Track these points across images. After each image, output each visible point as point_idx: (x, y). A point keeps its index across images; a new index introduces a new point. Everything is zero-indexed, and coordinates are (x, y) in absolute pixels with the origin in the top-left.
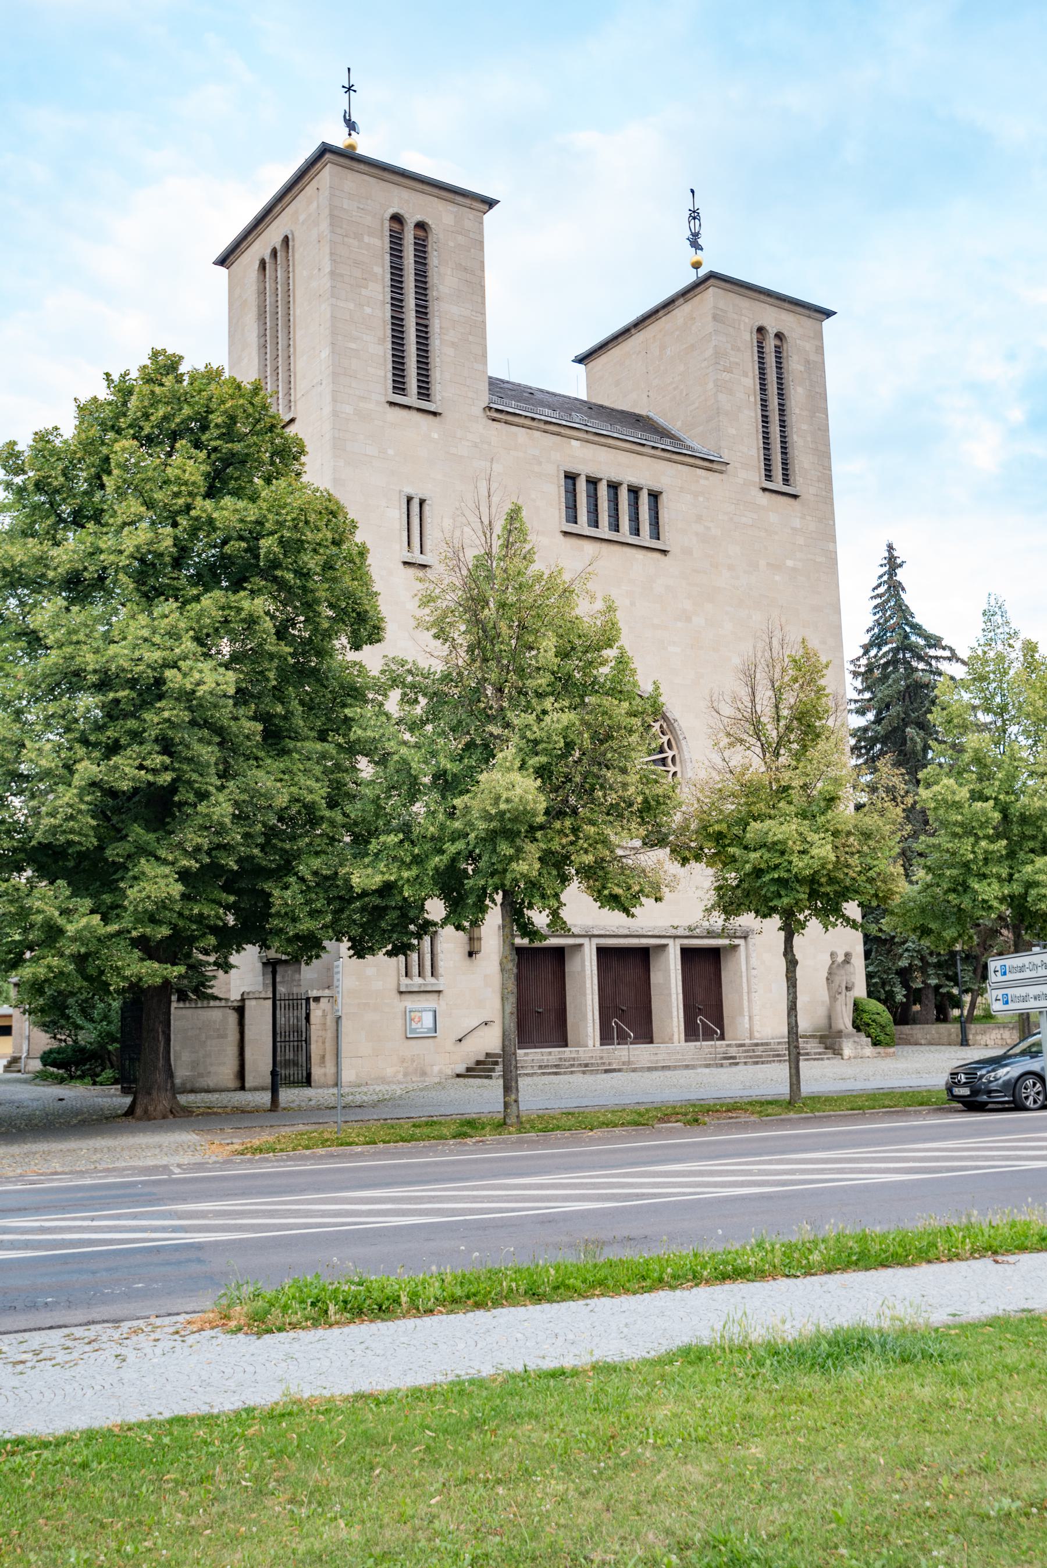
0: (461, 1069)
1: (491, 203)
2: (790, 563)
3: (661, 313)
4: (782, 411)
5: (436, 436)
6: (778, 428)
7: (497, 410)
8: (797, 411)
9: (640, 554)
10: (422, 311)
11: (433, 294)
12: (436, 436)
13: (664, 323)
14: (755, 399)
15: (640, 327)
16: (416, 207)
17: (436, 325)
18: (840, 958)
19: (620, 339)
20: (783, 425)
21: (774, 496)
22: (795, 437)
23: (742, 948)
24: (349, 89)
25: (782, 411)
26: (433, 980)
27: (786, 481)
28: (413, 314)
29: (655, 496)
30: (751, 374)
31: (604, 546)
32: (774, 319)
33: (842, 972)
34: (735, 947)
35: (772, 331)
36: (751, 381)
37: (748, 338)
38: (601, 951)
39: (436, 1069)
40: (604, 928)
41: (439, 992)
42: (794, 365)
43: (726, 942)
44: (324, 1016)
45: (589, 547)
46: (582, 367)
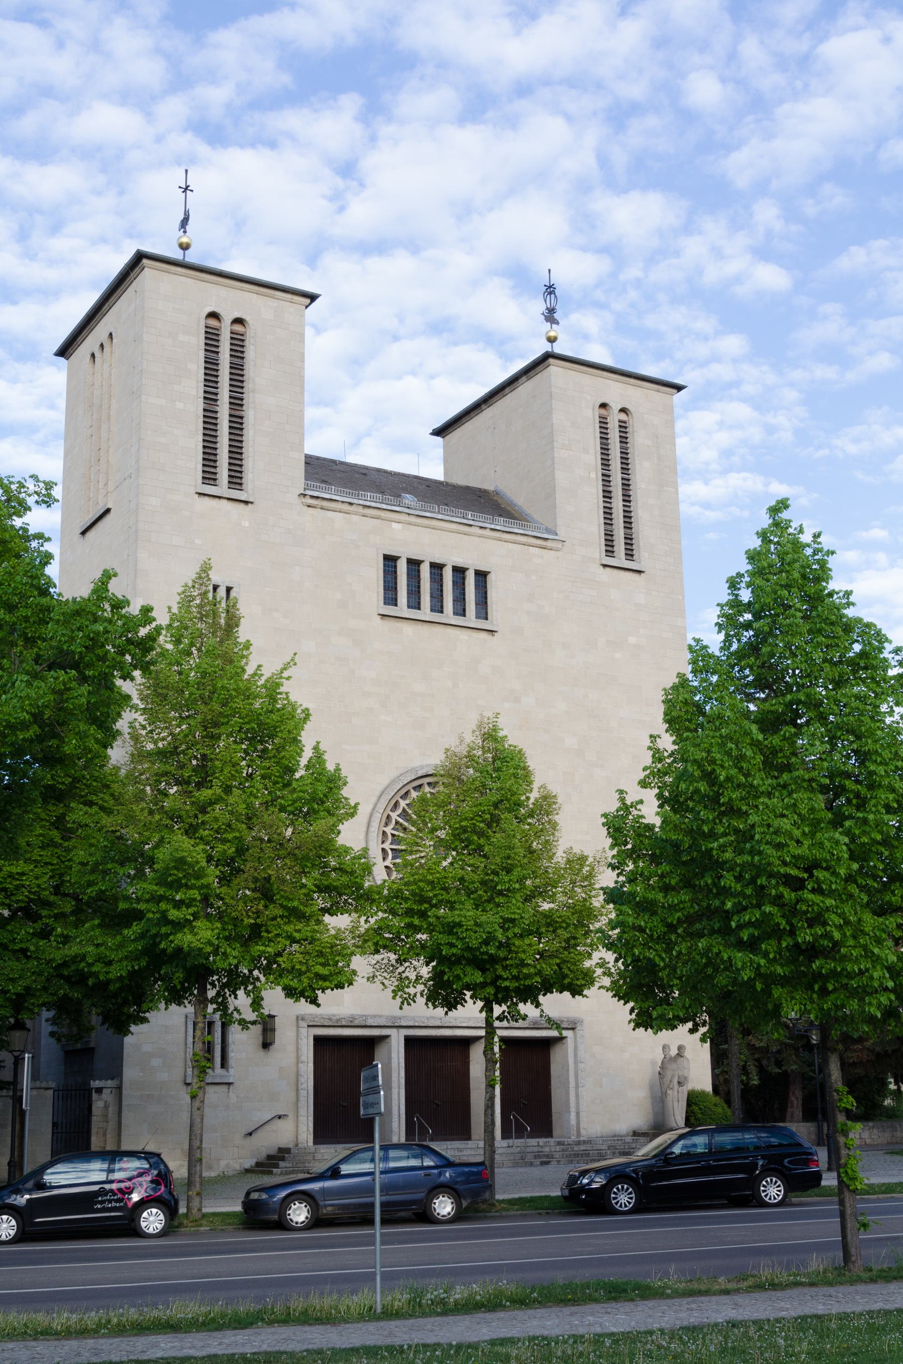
0: (249, 1163)
1: (313, 298)
2: (632, 640)
3: (507, 390)
4: (626, 486)
5: (247, 524)
6: (621, 503)
7: (312, 497)
8: (643, 486)
9: (464, 635)
10: (237, 402)
11: (248, 386)
12: (247, 524)
13: (100, 525)
14: (596, 475)
15: (490, 402)
16: (230, 302)
17: (251, 416)
18: (674, 1052)
19: (472, 414)
20: (627, 498)
21: (616, 571)
22: (640, 512)
23: (570, 1042)
24: (186, 189)
25: (626, 486)
26: (223, 1072)
27: (630, 555)
28: (227, 406)
29: (482, 576)
30: (592, 451)
31: (426, 627)
32: (618, 393)
33: (674, 1066)
34: (561, 1039)
35: (615, 406)
36: (594, 457)
37: (591, 415)
38: (409, 1040)
39: (223, 1163)
40: (413, 1018)
41: (229, 1084)
42: (639, 440)
43: (554, 1033)
44: (106, 1107)
45: (408, 629)
46: (439, 439)
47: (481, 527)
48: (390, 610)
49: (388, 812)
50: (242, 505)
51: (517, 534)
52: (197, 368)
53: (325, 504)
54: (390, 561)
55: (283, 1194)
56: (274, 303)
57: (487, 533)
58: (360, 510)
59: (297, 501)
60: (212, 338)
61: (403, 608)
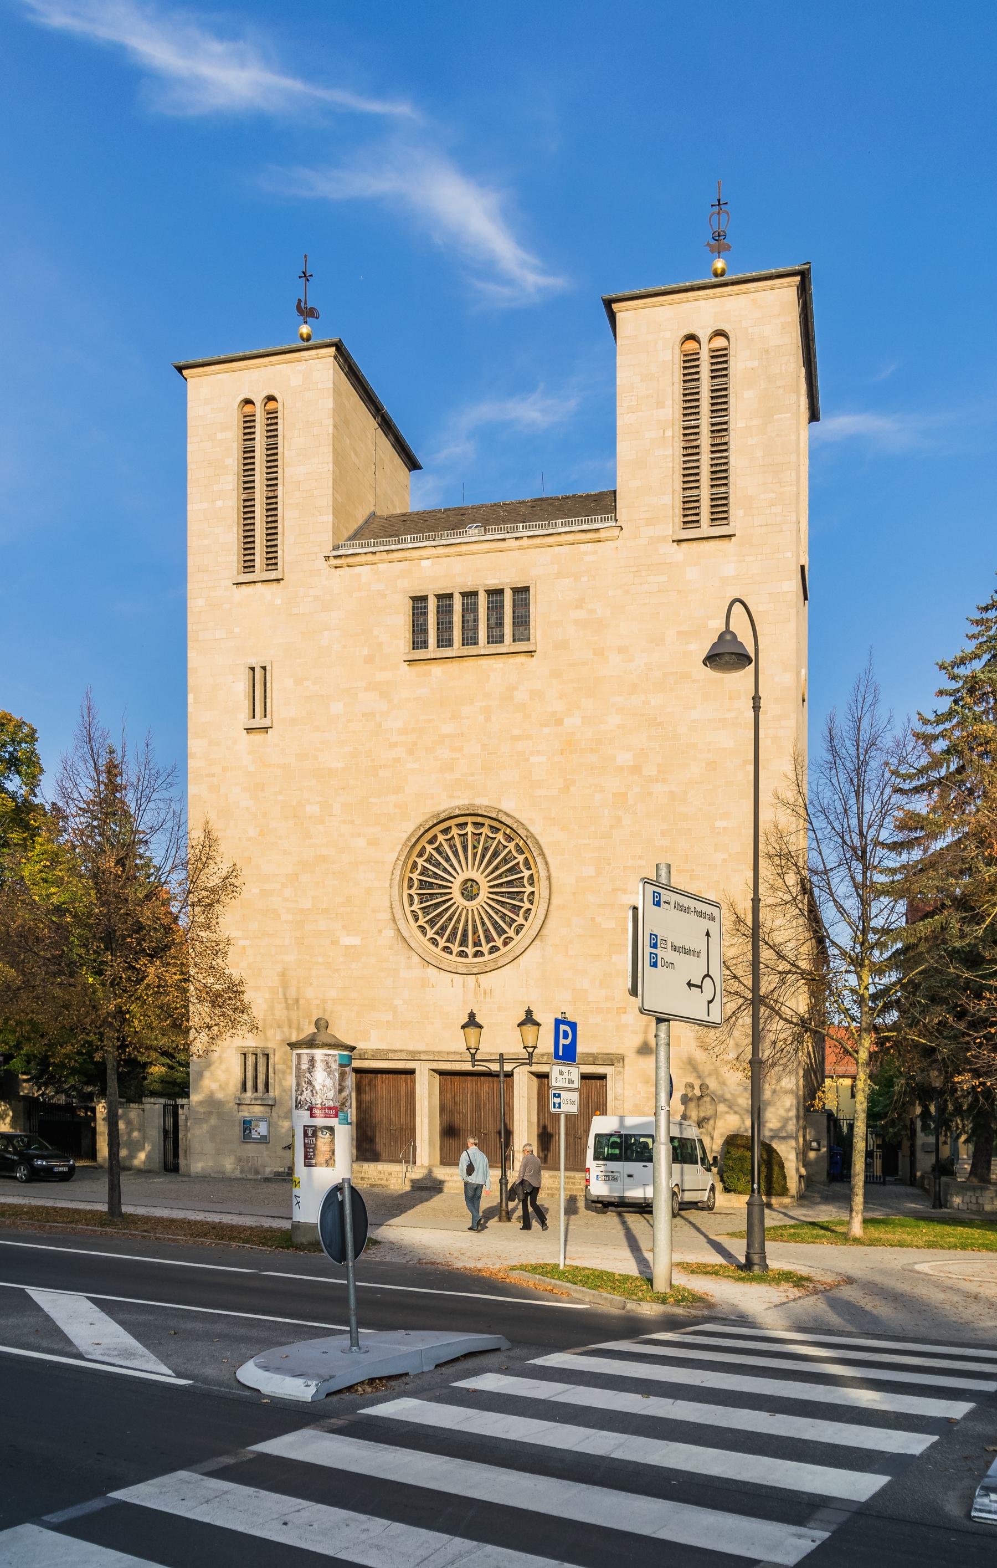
10: (272, 483)
21: (695, 544)
47: (517, 538)
48: (420, 654)
49: (527, 855)
50: (275, 584)
51: (347, 556)
52: (233, 461)
53: (350, 560)
54: (419, 601)
55: (530, 1209)
56: (301, 367)
57: (526, 542)
58: (384, 555)
59: (321, 563)
60: (690, 363)
61: (432, 649)
